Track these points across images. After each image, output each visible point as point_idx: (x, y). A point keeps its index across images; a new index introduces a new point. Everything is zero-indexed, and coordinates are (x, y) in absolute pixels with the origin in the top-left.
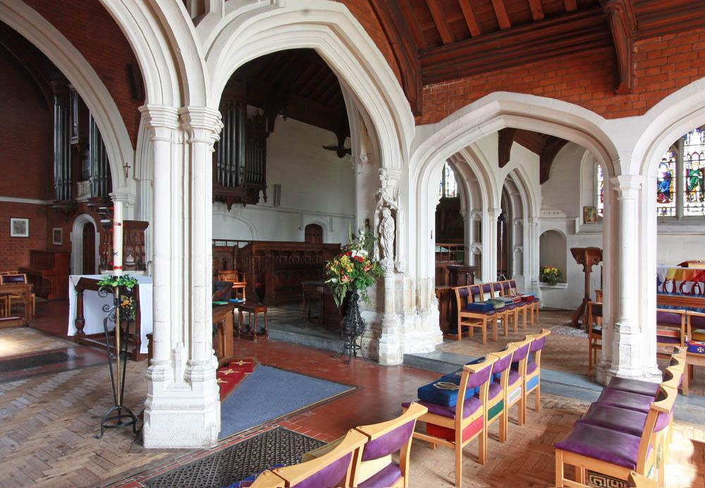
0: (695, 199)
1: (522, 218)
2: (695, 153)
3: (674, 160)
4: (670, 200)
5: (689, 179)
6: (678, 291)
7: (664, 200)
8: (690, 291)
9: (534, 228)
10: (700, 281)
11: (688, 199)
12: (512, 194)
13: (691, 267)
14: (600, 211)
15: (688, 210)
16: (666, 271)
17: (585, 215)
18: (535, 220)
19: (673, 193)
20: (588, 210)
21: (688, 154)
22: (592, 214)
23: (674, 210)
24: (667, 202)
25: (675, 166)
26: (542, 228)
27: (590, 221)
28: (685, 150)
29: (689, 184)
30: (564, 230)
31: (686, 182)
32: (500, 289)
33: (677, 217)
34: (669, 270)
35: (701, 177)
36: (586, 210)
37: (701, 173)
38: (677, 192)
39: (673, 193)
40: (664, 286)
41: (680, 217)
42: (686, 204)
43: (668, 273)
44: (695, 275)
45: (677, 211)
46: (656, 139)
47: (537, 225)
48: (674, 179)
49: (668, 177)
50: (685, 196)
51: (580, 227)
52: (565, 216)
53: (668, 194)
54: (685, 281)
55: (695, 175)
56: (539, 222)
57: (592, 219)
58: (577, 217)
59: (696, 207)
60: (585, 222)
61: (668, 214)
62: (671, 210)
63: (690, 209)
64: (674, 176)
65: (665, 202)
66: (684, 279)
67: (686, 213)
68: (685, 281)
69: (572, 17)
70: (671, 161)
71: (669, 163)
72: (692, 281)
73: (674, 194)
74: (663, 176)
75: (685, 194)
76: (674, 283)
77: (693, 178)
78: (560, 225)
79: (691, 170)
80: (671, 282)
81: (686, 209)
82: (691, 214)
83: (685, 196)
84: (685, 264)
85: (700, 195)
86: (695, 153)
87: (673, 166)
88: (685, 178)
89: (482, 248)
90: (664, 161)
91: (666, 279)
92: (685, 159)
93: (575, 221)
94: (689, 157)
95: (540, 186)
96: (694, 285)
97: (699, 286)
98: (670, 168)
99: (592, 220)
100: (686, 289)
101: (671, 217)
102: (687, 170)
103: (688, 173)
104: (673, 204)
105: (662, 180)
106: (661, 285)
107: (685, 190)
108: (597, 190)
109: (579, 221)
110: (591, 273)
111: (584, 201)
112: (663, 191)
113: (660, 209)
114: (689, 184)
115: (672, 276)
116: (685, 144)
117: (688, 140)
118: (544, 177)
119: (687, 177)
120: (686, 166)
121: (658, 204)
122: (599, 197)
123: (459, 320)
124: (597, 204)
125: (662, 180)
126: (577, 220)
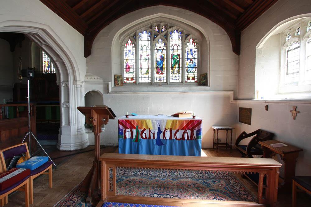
0: (175, 72)
1: (68, 81)
2: (175, 45)
3: (165, 48)
4: (163, 73)
5: (172, 60)
6: (173, 138)
7: (160, 73)
8: (181, 137)
9: (79, 89)
10: (188, 129)
11: (172, 72)
12: (57, 61)
13: (181, 117)
14: (125, 79)
15: (172, 79)
16: (165, 122)
17: (116, 80)
18: (79, 83)
19: (164, 68)
20: (118, 77)
21: (172, 45)
22: (120, 80)
23: (165, 78)
24: (162, 73)
25: (165, 52)
26: (86, 89)
27: (118, 84)
28: (171, 43)
29: (173, 63)
30: (101, 91)
31: (171, 62)
32: (193, 118)
33: (167, 82)
34: (167, 121)
35: (178, 59)
36: (116, 77)
37: (178, 57)
38: (167, 68)
39: (164, 68)
40: (164, 135)
41: (168, 83)
42: (171, 75)
43: (167, 124)
44: (185, 125)
45: (167, 79)
46: (50, 28)
47: (81, 86)
48: (165, 60)
49: (162, 59)
50: (171, 70)
51: (112, 88)
52: (102, 81)
53: (162, 68)
54: (178, 130)
55: (175, 58)
56: (83, 85)
57: (120, 83)
58: (109, 82)
59: (176, 77)
60: (115, 85)
61: (162, 81)
62: (163, 79)
63: (142, 78)
64: (165, 58)
65: (160, 74)
66: (177, 127)
67: (171, 81)
68: (178, 130)
69: (260, 6)
70: (164, 49)
71: (163, 50)
72: (183, 129)
73: (165, 69)
74: (159, 58)
75: (171, 69)
76: (171, 131)
77: (175, 60)
78: (99, 87)
79: (173, 55)
80: (169, 130)
81: (140, 78)
82: (174, 81)
83: (171, 70)
84: (176, 115)
85: (178, 70)
86: (175, 45)
87: (165, 52)
88: (170, 60)
89: (69, 105)
90: (160, 49)
91: (165, 128)
92: (171, 48)
93: (108, 84)
94: (172, 46)
95: (85, 59)
96: (184, 133)
97: (187, 133)
98: (163, 53)
99: (120, 84)
100: (179, 136)
101: (164, 82)
102: (172, 55)
103: (172, 57)
104: (165, 75)
105: (159, 60)
106: (162, 134)
107: (170, 67)
108: (123, 65)
109: (111, 85)
110: (101, 133)
111: (115, 71)
112: (159, 67)
113: (158, 78)
114: (173, 63)
115: (169, 126)
116: (140, 40)
117: (172, 37)
118: (87, 52)
119: (172, 59)
120: (171, 52)
121: (157, 74)
122: (125, 70)
123: (134, 157)
124: (123, 74)
125: (159, 60)
126: (110, 83)
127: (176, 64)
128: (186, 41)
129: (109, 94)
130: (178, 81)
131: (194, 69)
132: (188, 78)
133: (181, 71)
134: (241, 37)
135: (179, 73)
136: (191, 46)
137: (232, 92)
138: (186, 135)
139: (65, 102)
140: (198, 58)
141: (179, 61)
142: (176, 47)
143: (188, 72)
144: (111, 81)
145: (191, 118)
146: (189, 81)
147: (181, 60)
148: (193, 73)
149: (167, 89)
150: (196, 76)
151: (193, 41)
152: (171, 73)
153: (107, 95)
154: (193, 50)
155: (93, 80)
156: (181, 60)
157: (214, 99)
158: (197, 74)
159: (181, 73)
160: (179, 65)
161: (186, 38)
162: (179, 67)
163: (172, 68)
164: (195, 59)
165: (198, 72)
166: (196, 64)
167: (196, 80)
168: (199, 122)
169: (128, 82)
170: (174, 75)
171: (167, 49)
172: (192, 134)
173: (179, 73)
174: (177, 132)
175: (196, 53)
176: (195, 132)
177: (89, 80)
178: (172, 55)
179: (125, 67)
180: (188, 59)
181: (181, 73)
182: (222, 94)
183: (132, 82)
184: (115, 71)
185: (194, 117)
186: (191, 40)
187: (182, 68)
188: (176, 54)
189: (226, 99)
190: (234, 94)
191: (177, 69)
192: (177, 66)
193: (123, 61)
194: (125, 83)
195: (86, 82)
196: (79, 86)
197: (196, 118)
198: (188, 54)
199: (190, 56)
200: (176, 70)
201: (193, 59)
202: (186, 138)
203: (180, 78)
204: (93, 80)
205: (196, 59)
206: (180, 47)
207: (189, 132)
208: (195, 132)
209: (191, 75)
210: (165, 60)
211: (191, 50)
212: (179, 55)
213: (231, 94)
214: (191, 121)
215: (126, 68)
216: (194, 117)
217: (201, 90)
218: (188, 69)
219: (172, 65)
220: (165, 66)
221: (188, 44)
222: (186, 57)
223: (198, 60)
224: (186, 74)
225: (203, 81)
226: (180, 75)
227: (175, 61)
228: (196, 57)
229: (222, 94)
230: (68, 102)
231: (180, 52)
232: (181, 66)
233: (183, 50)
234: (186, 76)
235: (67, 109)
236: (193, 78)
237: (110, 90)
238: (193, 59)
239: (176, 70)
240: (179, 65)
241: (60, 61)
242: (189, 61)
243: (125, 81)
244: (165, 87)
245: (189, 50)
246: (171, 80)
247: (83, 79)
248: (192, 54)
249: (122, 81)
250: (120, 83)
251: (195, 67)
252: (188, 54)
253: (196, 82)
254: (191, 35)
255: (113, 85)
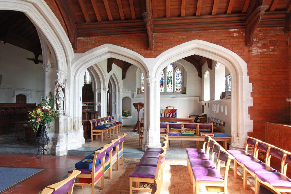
1: (116, 92)
3: (164, 73)
6: (165, 116)
13: (169, 108)
14: (142, 90)
17: (138, 91)
18: (121, 93)
23: (164, 90)
24: (162, 87)
26: (123, 96)
38: (165, 84)
42: (167, 88)
43: (163, 110)
44: (170, 111)
47: (121, 94)
48: (164, 80)
50: (167, 85)
51: (136, 95)
55: (170, 78)
56: (122, 94)
57: (140, 93)
60: (137, 94)
66: (167, 112)
70: (163, 74)
78: (129, 95)
80: (163, 113)
83: (167, 85)
87: (164, 75)
93: (134, 93)
95: (122, 80)
98: (163, 76)
100: (168, 115)
103: (168, 78)
104: (164, 88)
107: (167, 83)
108: (141, 82)
109: (136, 93)
111: (137, 86)
114: (168, 81)
115: (164, 112)
118: (124, 77)
119: (167, 79)
120: (167, 75)
122: (142, 85)
126: (135, 93)
127: (169, 82)
128: (175, 70)
129: (134, 99)
130: (171, 91)
131: (180, 84)
132: (177, 90)
133: (173, 85)
134: (202, 69)
135: (171, 86)
136: (178, 72)
137: (199, 97)
138: (170, 115)
139: (114, 102)
140: (182, 79)
141: (171, 80)
142: (170, 73)
143: (176, 86)
144: (135, 91)
145: (173, 108)
146: (177, 91)
147: (173, 80)
148: (180, 87)
149: (165, 96)
150: (181, 88)
151: (179, 69)
152: (167, 86)
153: (133, 99)
154: (179, 75)
155: (126, 91)
156: (173, 80)
157: (190, 101)
158: (182, 87)
159: (172, 86)
160: (172, 82)
161: (175, 68)
162: (172, 84)
163: (168, 84)
164: (180, 79)
165: (182, 86)
166: (181, 82)
167: (181, 90)
168: (176, 110)
169: (177, 91)
170: (169, 88)
171: (165, 74)
172: (173, 115)
173: (171, 86)
174: (166, 114)
175: (181, 76)
176: (174, 114)
177: (125, 91)
178: (168, 77)
179: (142, 84)
180: (176, 79)
181: (172, 86)
182: (193, 98)
183: (180, 91)
184: (137, 86)
185: (174, 108)
186: (178, 69)
187: (173, 84)
188: (170, 77)
189: (195, 101)
190: (200, 98)
191: (171, 84)
192: (170, 83)
193: (141, 81)
194: (142, 92)
195: (123, 92)
196: (120, 94)
197: (175, 109)
198: (176, 76)
199: (178, 78)
200: (170, 85)
201: (179, 79)
202: (170, 116)
203: (172, 89)
204: (126, 91)
205: (181, 79)
206: (172, 73)
207: (172, 114)
208: (174, 114)
209: (178, 88)
210: (164, 80)
211: (178, 74)
212: (171, 77)
213: (198, 98)
214: (173, 110)
215: (143, 84)
216: (174, 108)
217: (182, 96)
218: (177, 84)
219: (168, 82)
220: (164, 83)
221: (176, 71)
222: (175, 78)
223: (182, 80)
224: (176, 87)
225: (184, 91)
226: (172, 88)
227: (169, 80)
228: (181, 78)
229: (193, 98)
230: (116, 102)
231: (172, 75)
232: (173, 83)
233: (174, 74)
234: (176, 88)
235: (115, 106)
236: (180, 90)
237: (135, 96)
238: (179, 79)
239: (170, 85)
240: (172, 82)
241: (114, 83)
242: (177, 80)
243: (176, 91)
244: (164, 94)
245: (177, 74)
246: (167, 91)
247: (122, 91)
248: (179, 76)
249: (141, 91)
250: (140, 93)
251: (180, 83)
252: (176, 76)
253: (181, 92)
254: (178, 67)
255: (136, 94)
